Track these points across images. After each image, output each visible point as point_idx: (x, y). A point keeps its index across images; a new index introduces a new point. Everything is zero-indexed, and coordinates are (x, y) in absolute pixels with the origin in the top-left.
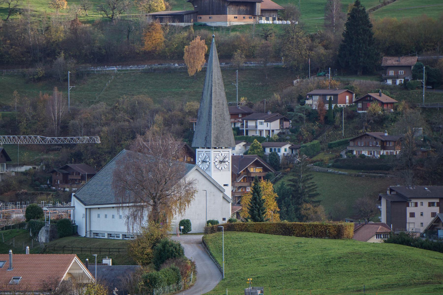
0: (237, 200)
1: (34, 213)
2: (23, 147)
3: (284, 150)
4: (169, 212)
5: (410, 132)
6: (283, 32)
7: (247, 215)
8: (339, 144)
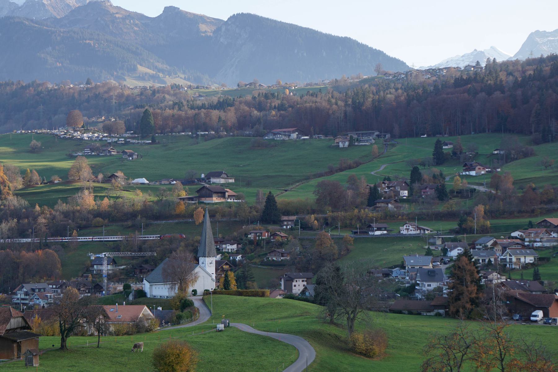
0: (218, 280)
1: (127, 287)
2: (122, 258)
3: (239, 258)
4: (187, 286)
5: (293, 249)
6: (238, 205)
7: (222, 287)
8: (263, 255)
